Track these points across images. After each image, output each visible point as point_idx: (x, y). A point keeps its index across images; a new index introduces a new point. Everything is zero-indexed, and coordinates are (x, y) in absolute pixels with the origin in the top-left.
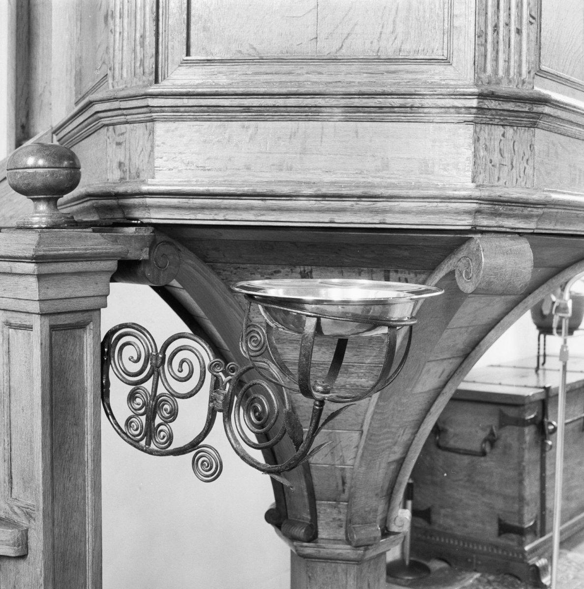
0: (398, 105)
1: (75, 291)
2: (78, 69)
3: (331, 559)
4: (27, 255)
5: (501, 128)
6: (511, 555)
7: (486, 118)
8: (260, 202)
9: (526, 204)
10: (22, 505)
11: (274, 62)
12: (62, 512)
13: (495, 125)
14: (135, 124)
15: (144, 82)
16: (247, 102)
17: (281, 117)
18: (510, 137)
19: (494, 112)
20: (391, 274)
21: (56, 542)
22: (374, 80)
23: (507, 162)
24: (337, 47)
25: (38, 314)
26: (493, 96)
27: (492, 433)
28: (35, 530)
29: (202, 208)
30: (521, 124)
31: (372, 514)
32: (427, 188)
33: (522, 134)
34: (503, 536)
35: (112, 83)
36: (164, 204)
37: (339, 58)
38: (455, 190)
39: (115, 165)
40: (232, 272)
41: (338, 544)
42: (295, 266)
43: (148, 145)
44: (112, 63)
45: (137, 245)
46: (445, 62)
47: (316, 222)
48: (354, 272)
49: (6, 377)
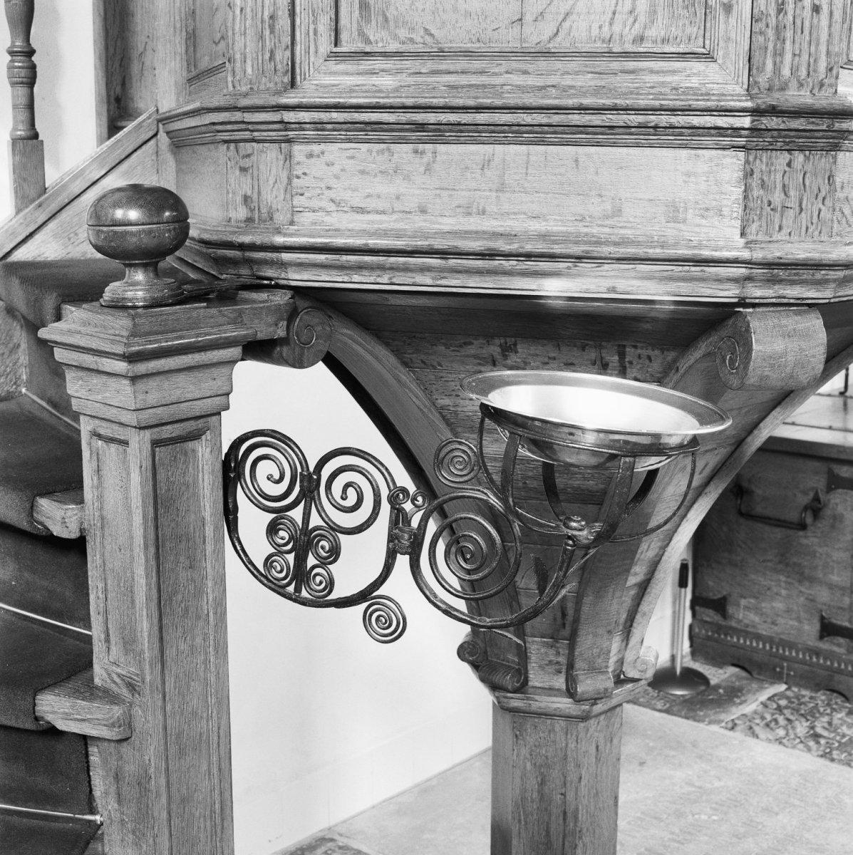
0: (636, 124)
1: (187, 390)
2: (190, 29)
3: (546, 715)
4: (117, 352)
5: (786, 154)
6: (836, 665)
7: (764, 141)
8: (439, 261)
9: (818, 266)
10: (124, 673)
11: (460, 56)
12: (175, 682)
13: (776, 150)
14: (265, 144)
15: (276, 84)
16: (420, 117)
17: (469, 138)
18: (800, 167)
19: (775, 133)
20: (628, 349)
21: (169, 722)
22: (603, 83)
23: (793, 202)
24: (551, 34)
25: (135, 427)
26: (773, 111)
27: (816, 499)
28: (140, 706)
29: (360, 267)
30: (816, 147)
31: (602, 657)
32: (676, 245)
33: (816, 162)
34: (826, 639)
35: (233, 82)
36: (307, 261)
37: (553, 50)
38: (716, 251)
39: (239, 199)
40: (404, 342)
41: (555, 696)
42: (492, 337)
43: (284, 175)
44: (231, 51)
45: (270, 320)
46: (705, 58)
47: (519, 289)
48: (575, 346)
49: (96, 504)
